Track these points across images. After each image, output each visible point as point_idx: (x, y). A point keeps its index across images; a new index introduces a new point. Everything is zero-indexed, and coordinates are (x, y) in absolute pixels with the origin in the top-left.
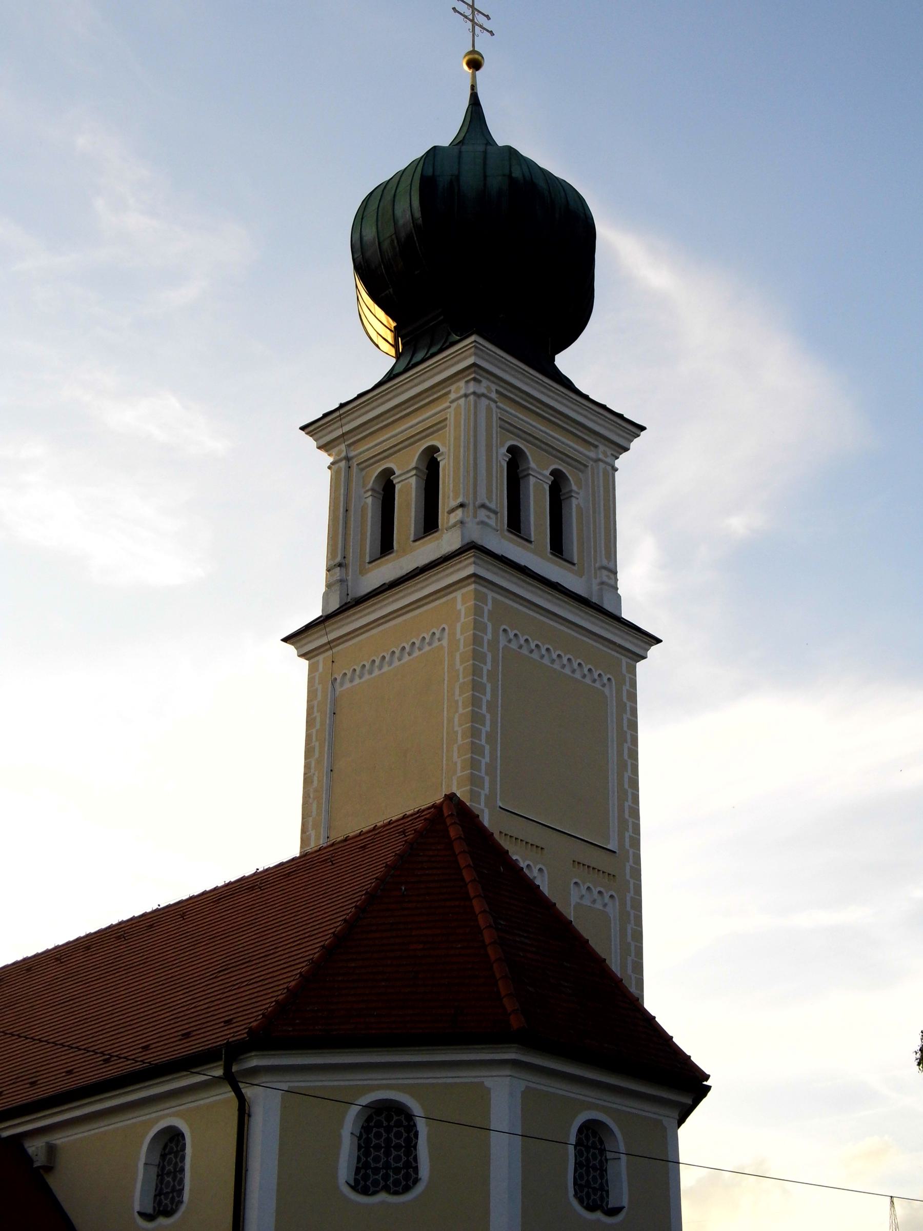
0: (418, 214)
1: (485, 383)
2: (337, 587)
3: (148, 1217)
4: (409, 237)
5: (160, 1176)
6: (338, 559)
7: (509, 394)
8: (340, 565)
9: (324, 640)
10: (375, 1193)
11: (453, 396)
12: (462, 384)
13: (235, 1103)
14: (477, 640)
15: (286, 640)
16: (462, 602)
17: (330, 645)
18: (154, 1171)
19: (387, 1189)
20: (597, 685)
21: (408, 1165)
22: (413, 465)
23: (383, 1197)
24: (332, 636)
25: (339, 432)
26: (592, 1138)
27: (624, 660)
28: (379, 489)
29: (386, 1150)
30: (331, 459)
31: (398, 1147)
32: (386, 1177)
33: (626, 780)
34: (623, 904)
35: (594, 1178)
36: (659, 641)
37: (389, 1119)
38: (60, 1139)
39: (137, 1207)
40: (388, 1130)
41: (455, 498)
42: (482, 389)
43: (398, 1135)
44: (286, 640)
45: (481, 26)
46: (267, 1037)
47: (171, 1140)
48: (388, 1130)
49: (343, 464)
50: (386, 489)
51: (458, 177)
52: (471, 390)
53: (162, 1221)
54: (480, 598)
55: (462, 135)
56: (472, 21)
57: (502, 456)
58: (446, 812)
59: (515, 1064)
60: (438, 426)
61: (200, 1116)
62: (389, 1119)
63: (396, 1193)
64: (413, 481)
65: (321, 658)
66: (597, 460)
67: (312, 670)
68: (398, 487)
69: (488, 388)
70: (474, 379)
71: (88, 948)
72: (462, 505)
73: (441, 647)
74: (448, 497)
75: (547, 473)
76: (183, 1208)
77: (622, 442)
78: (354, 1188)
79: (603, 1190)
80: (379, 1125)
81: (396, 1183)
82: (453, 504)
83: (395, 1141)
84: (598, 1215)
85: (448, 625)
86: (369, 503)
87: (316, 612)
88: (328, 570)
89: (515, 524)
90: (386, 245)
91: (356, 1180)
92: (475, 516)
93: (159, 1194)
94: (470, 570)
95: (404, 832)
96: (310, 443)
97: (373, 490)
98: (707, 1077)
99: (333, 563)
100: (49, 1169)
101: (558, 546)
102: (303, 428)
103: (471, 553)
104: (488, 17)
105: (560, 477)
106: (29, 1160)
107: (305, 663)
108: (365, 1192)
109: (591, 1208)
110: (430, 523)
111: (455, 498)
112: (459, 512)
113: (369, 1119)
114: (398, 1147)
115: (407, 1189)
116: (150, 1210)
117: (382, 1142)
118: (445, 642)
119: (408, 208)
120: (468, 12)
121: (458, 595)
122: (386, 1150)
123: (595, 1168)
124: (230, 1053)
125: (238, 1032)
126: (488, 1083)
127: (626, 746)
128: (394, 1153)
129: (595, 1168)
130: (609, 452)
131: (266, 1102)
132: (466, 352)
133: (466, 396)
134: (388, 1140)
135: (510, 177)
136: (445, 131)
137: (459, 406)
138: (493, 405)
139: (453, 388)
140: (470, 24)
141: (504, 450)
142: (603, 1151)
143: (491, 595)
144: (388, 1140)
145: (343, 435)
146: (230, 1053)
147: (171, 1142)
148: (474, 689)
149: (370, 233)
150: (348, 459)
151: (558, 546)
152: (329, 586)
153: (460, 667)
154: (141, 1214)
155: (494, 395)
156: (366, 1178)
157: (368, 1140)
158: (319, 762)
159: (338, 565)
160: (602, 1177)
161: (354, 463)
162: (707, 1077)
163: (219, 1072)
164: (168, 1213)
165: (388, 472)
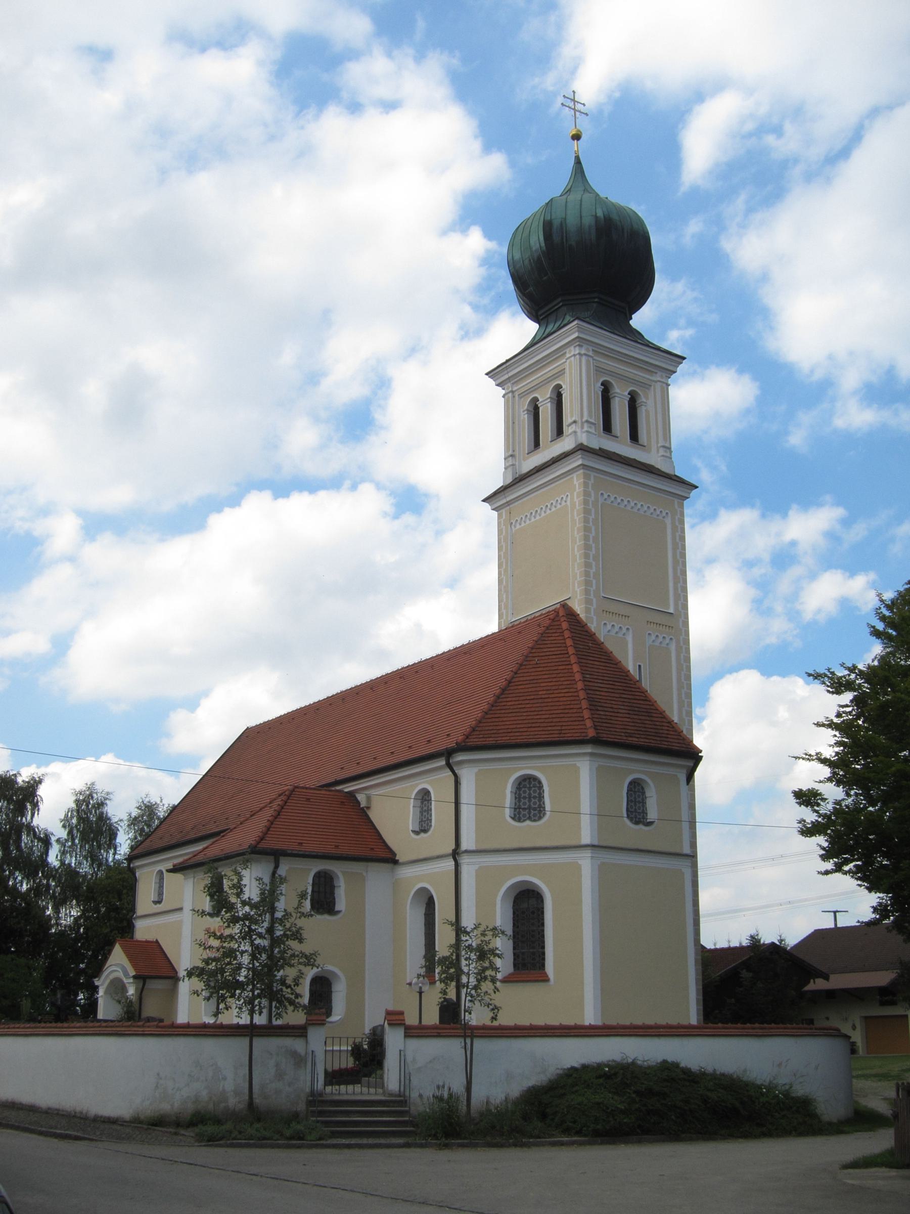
0: (543, 244)
1: (585, 346)
2: (510, 469)
3: (417, 833)
4: (539, 258)
5: (421, 812)
6: (510, 453)
7: (599, 350)
8: (511, 456)
9: (504, 501)
10: (524, 821)
11: (568, 355)
12: (572, 348)
13: (453, 778)
14: (586, 502)
15: (484, 501)
16: (577, 480)
17: (508, 503)
18: (418, 810)
19: (530, 818)
20: (660, 518)
21: (540, 806)
22: (548, 396)
23: (528, 822)
24: (508, 499)
25: (506, 377)
26: (636, 790)
27: (676, 501)
28: (531, 409)
29: (528, 800)
30: (504, 392)
31: (535, 797)
32: (529, 813)
33: (679, 571)
34: (678, 642)
35: (525, 804)
36: (696, 487)
37: (530, 783)
38: (373, 792)
39: (411, 828)
40: (530, 788)
41: (572, 416)
42: (583, 352)
43: (535, 791)
44: (484, 501)
45: (580, 112)
46: (463, 747)
47: (425, 794)
48: (530, 788)
49: (510, 395)
50: (535, 411)
51: (565, 219)
52: (577, 352)
53: (422, 835)
54: (586, 477)
55: (569, 187)
56: (574, 109)
57: (599, 388)
58: (561, 614)
59: (591, 754)
60: (561, 373)
61: (436, 782)
62: (530, 783)
63: (535, 821)
64: (549, 405)
65: (503, 511)
66: (656, 382)
67: (500, 517)
68: (541, 409)
69: (587, 350)
70: (579, 345)
71: (386, 683)
72: (575, 422)
73: (566, 506)
74: (567, 419)
75: (626, 393)
76: (432, 829)
77: (671, 368)
78: (513, 819)
79: (644, 813)
80: (525, 786)
81: (535, 815)
82: (570, 421)
83: (533, 795)
84: (641, 827)
85: (568, 498)
86: (525, 419)
87: (499, 484)
88: (505, 459)
89: (607, 427)
90: (527, 262)
91: (515, 815)
92: (582, 428)
93: (421, 821)
94: (580, 462)
95: (539, 625)
96: (491, 382)
97: (527, 410)
98: (701, 751)
99: (507, 454)
100: (368, 808)
101: (634, 436)
102: (487, 374)
103: (579, 452)
104: (584, 105)
105: (627, 408)
106: (358, 803)
107: (495, 513)
108: (519, 820)
109: (637, 823)
110: (559, 431)
111: (572, 416)
112: (574, 425)
113: (519, 784)
114: (535, 797)
115: (540, 818)
116: (417, 829)
117: (527, 795)
118: (568, 503)
119: (537, 240)
120: (571, 105)
121: (575, 476)
122: (528, 800)
123: (639, 802)
124: (448, 754)
125: (451, 743)
126: (578, 764)
127: (678, 551)
128: (523, 801)
129: (639, 802)
130: (664, 375)
131: (468, 776)
132: (572, 330)
133: (574, 355)
134: (530, 794)
135: (596, 217)
136: (557, 183)
137: (570, 362)
138: (591, 360)
139: (567, 350)
140: (573, 112)
141: (599, 384)
142: (644, 793)
143: (593, 474)
144: (530, 794)
145: (509, 378)
146: (448, 754)
147: (424, 796)
148: (585, 531)
149: (517, 256)
150: (512, 392)
151: (634, 436)
152: (506, 468)
153: (577, 518)
154: (413, 831)
155: (591, 353)
156: (519, 813)
157: (520, 795)
158: (506, 571)
159: (510, 456)
160: (643, 806)
161: (516, 394)
162: (701, 751)
163: (443, 763)
164: (425, 831)
165: (535, 400)
